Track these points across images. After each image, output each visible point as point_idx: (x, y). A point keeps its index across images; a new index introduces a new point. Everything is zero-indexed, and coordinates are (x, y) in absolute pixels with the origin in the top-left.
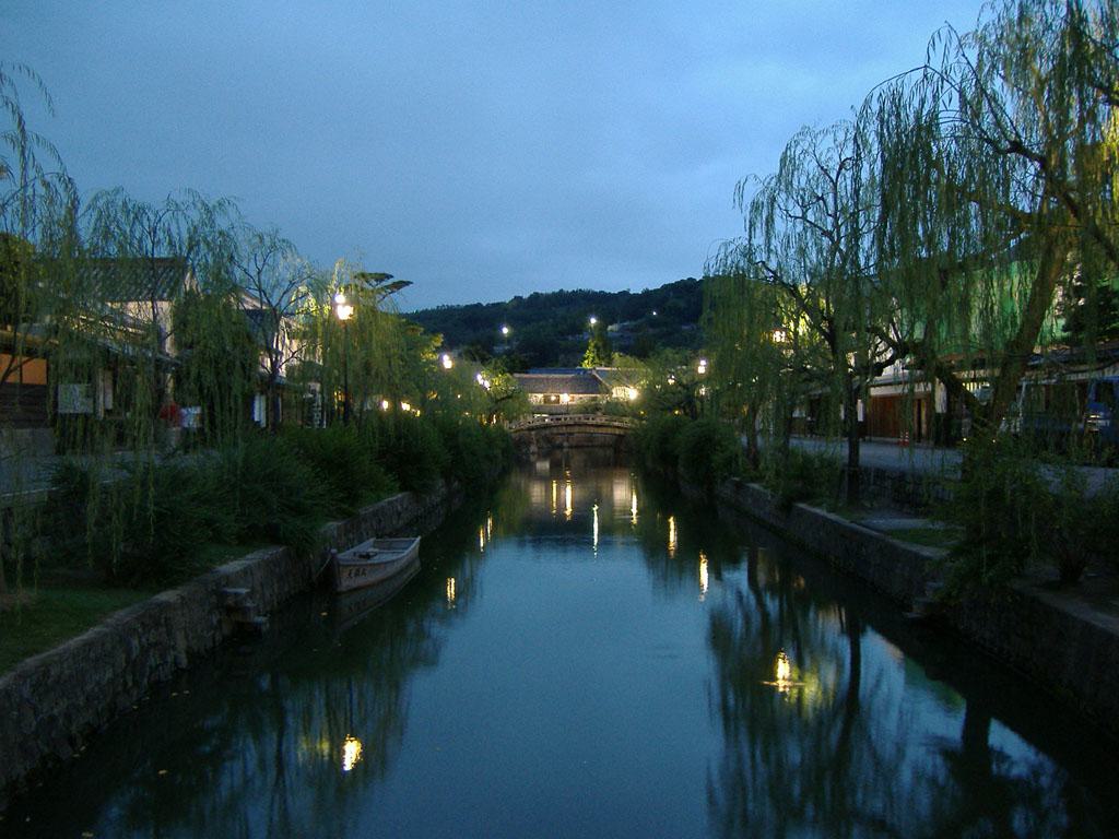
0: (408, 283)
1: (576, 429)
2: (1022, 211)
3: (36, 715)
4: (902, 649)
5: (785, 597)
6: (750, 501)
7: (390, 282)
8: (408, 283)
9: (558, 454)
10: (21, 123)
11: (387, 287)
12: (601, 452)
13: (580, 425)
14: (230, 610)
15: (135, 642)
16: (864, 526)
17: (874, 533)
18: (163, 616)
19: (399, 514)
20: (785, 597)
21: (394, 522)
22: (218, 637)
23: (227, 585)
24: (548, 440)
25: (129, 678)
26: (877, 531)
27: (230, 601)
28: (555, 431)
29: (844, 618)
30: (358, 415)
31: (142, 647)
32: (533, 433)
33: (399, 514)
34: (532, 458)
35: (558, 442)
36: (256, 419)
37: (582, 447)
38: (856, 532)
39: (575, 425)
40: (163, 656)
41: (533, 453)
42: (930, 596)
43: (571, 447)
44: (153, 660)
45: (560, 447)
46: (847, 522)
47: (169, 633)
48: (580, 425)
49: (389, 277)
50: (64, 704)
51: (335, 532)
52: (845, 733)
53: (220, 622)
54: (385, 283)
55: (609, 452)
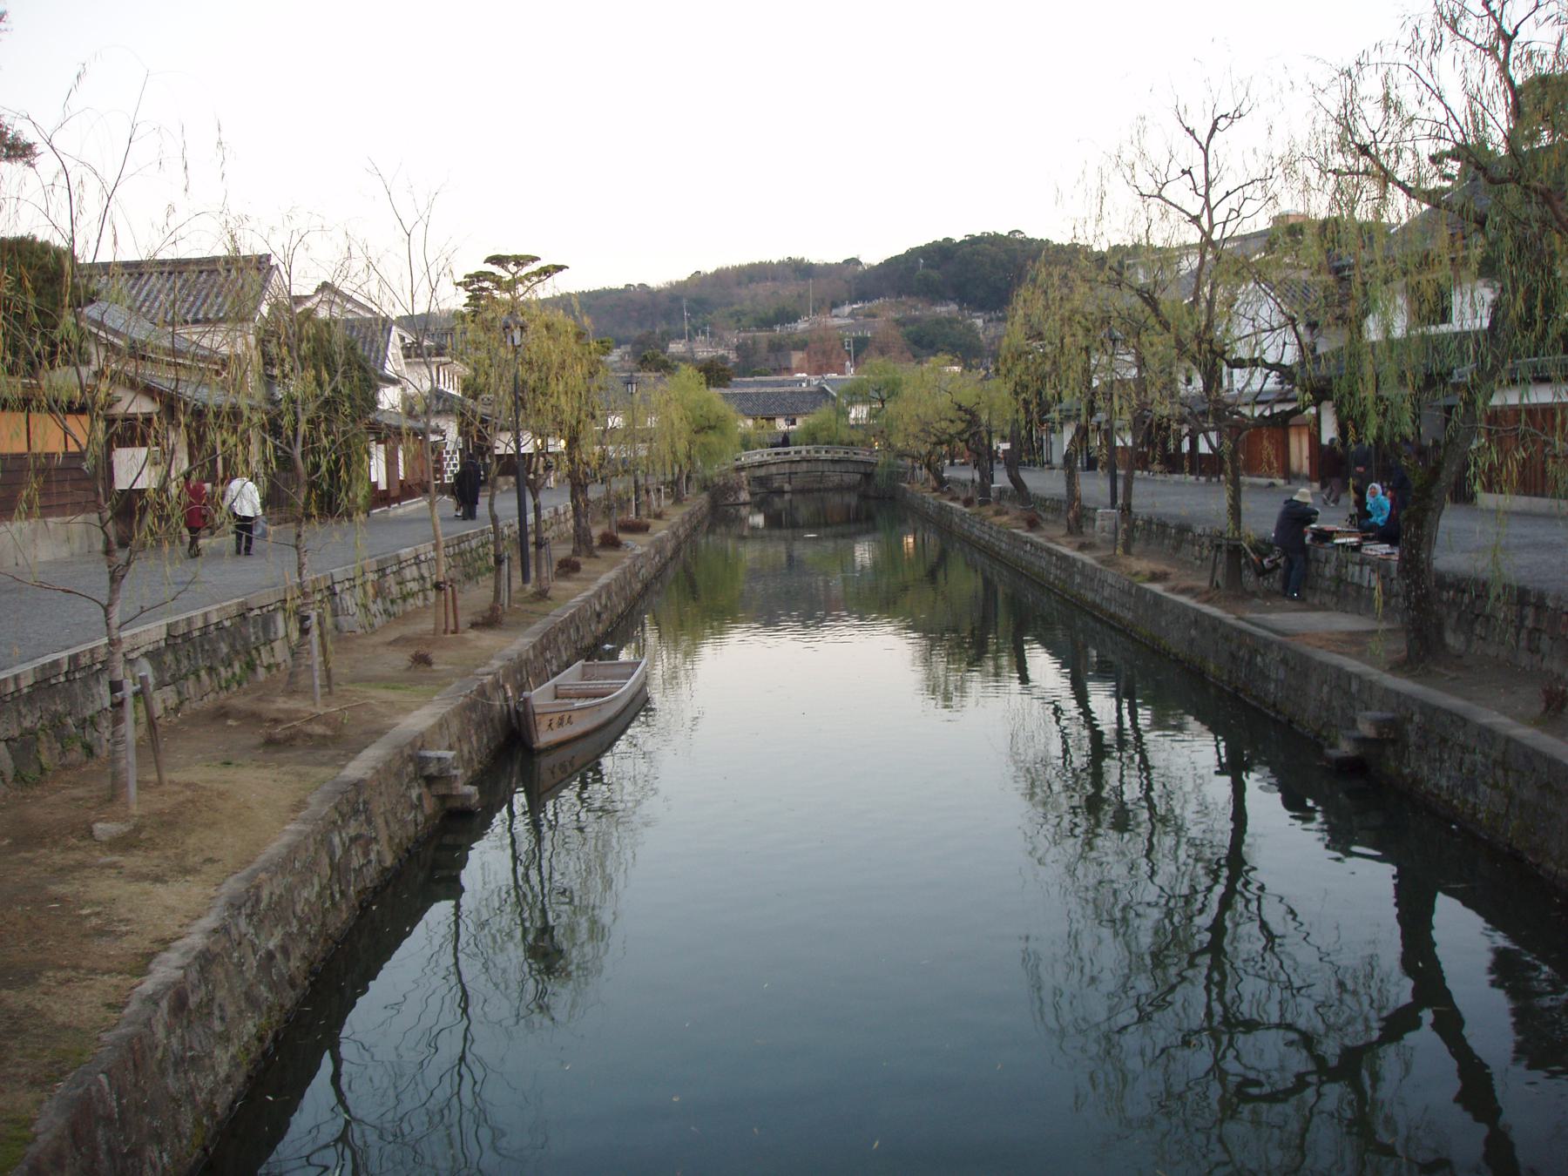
0: (559, 268)
1: (804, 466)
2: (1494, 152)
3: (255, 953)
4: (1480, 912)
5: (1125, 705)
6: (1078, 579)
7: (534, 267)
8: (559, 268)
9: (778, 503)
10: (1295, 960)
11: (534, 274)
12: (835, 500)
13: (809, 461)
14: (430, 780)
15: (337, 840)
16: (1253, 624)
17: (1272, 636)
18: (361, 800)
19: (599, 615)
20: (1125, 705)
21: (593, 628)
22: (420, 818)
23: (422, 747)
24: (763, 481)
25: (336, 888)
26: (1276, 632)
27: (432, 769)
28: (773, 469)
29: (1223, 752)
30: (1194, 930)
31: (344, 844)
32: (743, 474)
33: (599, 615)
34: (744, 511)
35: (776, 485)
36: (374, 479)
37: (810, 491)
38: (1241, 632)
39: (803, 460)
40: (366, 854)
41: (744, 504)
42: (1366, 729)
43: (793, 492)
44: (356, 862)
45: (781, 492)
46: (1230, 619)
47: (369, 821)
48: (809, 461)
49: (535, 259)
50: (278, 933)
51: (531, 653)
52: (1226, 902)
53: (420, 797)
54: (526, 270)
55: (852, 499)
